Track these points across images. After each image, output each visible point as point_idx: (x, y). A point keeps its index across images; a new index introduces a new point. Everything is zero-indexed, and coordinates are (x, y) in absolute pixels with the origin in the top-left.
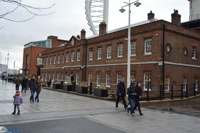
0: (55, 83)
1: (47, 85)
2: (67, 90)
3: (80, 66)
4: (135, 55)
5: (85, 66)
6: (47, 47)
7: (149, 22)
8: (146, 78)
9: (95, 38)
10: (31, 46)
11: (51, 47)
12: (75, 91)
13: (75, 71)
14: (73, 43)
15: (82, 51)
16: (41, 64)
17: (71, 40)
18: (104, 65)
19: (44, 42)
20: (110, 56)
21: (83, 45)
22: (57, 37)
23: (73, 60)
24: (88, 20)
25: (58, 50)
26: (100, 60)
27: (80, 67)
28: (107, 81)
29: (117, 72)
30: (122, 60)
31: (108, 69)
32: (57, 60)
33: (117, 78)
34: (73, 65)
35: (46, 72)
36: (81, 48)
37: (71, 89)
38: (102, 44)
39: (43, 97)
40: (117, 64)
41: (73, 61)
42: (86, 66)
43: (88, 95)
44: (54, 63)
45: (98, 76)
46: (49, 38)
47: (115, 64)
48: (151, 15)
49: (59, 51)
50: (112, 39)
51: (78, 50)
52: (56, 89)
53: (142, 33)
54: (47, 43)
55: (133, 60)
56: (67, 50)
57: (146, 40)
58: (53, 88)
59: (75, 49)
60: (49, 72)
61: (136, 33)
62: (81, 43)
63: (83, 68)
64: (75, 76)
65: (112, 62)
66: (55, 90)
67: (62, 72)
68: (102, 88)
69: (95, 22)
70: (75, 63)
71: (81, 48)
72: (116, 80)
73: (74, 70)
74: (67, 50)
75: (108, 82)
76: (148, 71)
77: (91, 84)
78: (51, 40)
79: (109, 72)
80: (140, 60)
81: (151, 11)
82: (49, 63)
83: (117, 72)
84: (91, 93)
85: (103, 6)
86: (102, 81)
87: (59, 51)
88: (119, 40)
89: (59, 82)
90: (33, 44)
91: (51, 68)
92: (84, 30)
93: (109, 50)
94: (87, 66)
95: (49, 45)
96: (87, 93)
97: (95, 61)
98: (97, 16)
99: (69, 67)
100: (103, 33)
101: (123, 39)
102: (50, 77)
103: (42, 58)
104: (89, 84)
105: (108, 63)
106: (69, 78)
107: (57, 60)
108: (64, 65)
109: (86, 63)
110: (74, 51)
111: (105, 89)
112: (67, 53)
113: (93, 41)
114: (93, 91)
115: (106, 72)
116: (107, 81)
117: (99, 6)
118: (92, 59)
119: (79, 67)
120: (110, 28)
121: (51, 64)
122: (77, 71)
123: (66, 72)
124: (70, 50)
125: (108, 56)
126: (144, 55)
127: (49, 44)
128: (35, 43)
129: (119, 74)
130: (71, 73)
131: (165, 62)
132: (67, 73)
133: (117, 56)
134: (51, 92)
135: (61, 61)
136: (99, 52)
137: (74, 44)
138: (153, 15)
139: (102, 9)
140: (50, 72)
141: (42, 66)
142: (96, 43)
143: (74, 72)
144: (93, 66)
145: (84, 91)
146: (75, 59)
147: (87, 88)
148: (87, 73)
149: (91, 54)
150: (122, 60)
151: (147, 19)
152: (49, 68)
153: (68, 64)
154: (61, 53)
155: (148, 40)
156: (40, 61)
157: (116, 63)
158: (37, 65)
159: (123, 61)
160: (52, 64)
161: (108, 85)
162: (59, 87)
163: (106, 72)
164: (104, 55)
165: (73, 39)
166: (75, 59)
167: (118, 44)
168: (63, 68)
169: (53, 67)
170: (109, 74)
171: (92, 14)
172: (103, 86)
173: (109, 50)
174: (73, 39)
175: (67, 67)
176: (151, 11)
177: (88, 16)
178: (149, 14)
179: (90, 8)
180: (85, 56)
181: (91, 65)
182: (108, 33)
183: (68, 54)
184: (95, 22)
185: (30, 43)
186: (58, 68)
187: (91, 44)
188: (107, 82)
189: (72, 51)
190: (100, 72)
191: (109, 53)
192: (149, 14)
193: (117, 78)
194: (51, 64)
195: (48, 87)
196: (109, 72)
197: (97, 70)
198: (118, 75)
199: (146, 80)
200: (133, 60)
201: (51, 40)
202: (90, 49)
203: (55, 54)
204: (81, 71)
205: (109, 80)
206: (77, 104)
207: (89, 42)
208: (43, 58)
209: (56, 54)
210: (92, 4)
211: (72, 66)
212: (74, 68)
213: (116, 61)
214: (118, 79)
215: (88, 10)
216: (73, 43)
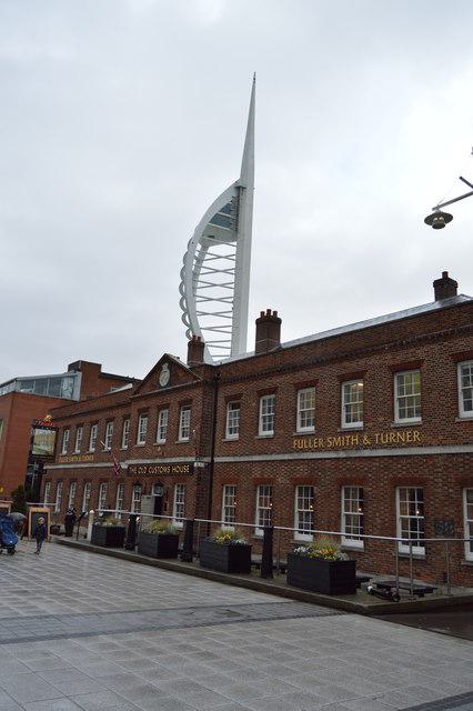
0: (105, 524)
1: (63, 528)
2: (155, 552)
3: (193, 459)
4: (417, 419)
5: (208, 459)
6: (67, 395)
7: (437, 306)
8: (300, 501)
9: (233, 363)
10: (14, 392)
11: (77, 397)
12: (190, 561)
13: (170, 479)
14: (164, 378)
15: (198, 406)
16: (49, 449)
17: (157, 370)
18: (286, 457)
19: (56, 381)
20: (270, 429)
21: (205, 383)
22: (166, 359)
23: (168, 438)
24: (187, 325)
25: (109, 405)
26: (268, 439)
27: (191, 464)
28: (343, 520)
29: (343, 482)
30: (361, 438)
31: (303, 471)
32: (102, 436)
33: (343, 507)
34: (162, 457)
35: (59, 481)
36: (197, 395)
37: (166, 551)
38: (277, 381)
39: (75, 594)
40: (342, 455)
41: (141, 443)
42: (213, 461)
43: (255, 579)
44: (92, 450)
45: (260, 498)
46: (72, 367)
47: (333, 455)
48: (269, 324)
49: (111, 408)
50: (319, 363)
51: (186, 404)
52: (107, 546)
53: (446, 337)
54: (66, 384)
55: (411, 438)
56: (143, 404)
57: (462, 364)
58: (92, 542)
59: (174, 400)
60: (70, 478)
61: (419, 340)
62: (189, 382)
63: (203, 465)
64: (168, 495)
65: (321, 443)
66: (97, 552)
67: (120, 481)
68: (331, 554)
69: (209, 329)
70: (173, 447)
71: (197, 395)
72: (255, 509)
73: (164, 475)
74: (143, 404)
75: (301, 519)
76: (413, 481)
77: (269, 532)
78: (80, 374)
79: (307, 485)
80: (441, 437)
81: (445, 274)
82: (71, 447)
83: (258, 482)
84: (267, 569)
85: (233, 286)
86: (322, 520)
87: (111, 408)
88: (346, 364)
89: (118, 516)
90: (19, 385)
91: (354, 454)
92: (275, 313)
93: (306, 402)
94: (217, 460)
95: (72, 391)
96: (175, 557)
97: (249, 440)
98: (216, 314)
99: (149, 462)
100: (270, 345)
101: (362, 362)
102: (71, 496)
103: (52, 429)
104: (260, 533)
105: (303, 450)
106: (149, 502)
107: (102, 436)
108: (128, 455)
109: (213, 448)
110: (167, 406)
111: (344, 557)
112: (143, 412)
113: (235, 371)
114: (260, 557)
115: (296, 482)
116: (343, 520)
117: (222, 285)
118: (235, 436)
119: (186, 463)
120: (288, 335)
121: (78, 451)
122: (179, 478)
123: (137, 480)
124: (153, 402)
125: (302, 426)
126: (457, 420)
127: (72, 385)
128: (26, 382)
129: (300, 489)
130: (159, 486)
131: (217, 460)
132: (138, 484)
133: (340, 425)
134: (86, 556)
135: (116, 442)
136: (163, 422)
137: (169, 384)
138: (454, 285)
139: (231, 293)
140: (73, 480)
141: (51, 458)
142: (252, 377)
143: (168, 482)
144: (274, 457)
145: (234, 564)
146: (172, 433)
147: (246, 550)
148: (216, 487)
149: (231, 418)
150: (361, 438)
151: (433, 299)
152: (71, 466)
153: (142, 452)
154: (119, 413)
155: (267, 397)
156: (43, 441)
157: (334, 449)
158: (34, 453)
159: (366, 441)
160: (82, 453)
161: (347, 537)
162: (115, 540)
163: (296, 482)
164: (284, 421)
165: (165, 366)
166: (172, 433)
167: (396, 369)
168: (124, 466)
169: (86, 462)
170: (305, 491)
171: (200, 307)
172: (324, 542)
173: (163, 422)
174: (165, 366)
175: (141, 462)
176: (445, 274)
177: (186, 312)
178: (437, 284)
179: (194, 288)
180: (209, 429)
181: (234, 455)
182: (283, 347)
183: (146, 416)
184: (209, 329)
185: (12, 382)
186: (109, 465)
187: (234, 381)
188: (399, 530)
189: (161, 408)
190: (270, 481)
191: (264, 417)
192: (437, 284)
193: (343, 507)
194: (80, 453)
195: (69, 533)
196: (307, 485)
197: (257, 473)
198: (300, 495)
199: (300, 507)
200: (411, 438)
201: (80, 374)
202: (228, 399)
203: (94, 417)
204: (194, 479)
205: (308, 513)
206: (71, 567)
207: (223, 374)
208: (56, 429)
209: (71, 422)
210: (201, 278)
211: (158, 461)
212: (165, 465)
213: (338, 441)
214: (258, 507)
215: (189, 295)
216: (164, 378)
